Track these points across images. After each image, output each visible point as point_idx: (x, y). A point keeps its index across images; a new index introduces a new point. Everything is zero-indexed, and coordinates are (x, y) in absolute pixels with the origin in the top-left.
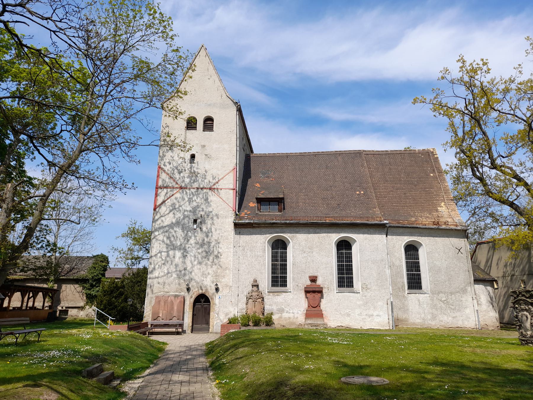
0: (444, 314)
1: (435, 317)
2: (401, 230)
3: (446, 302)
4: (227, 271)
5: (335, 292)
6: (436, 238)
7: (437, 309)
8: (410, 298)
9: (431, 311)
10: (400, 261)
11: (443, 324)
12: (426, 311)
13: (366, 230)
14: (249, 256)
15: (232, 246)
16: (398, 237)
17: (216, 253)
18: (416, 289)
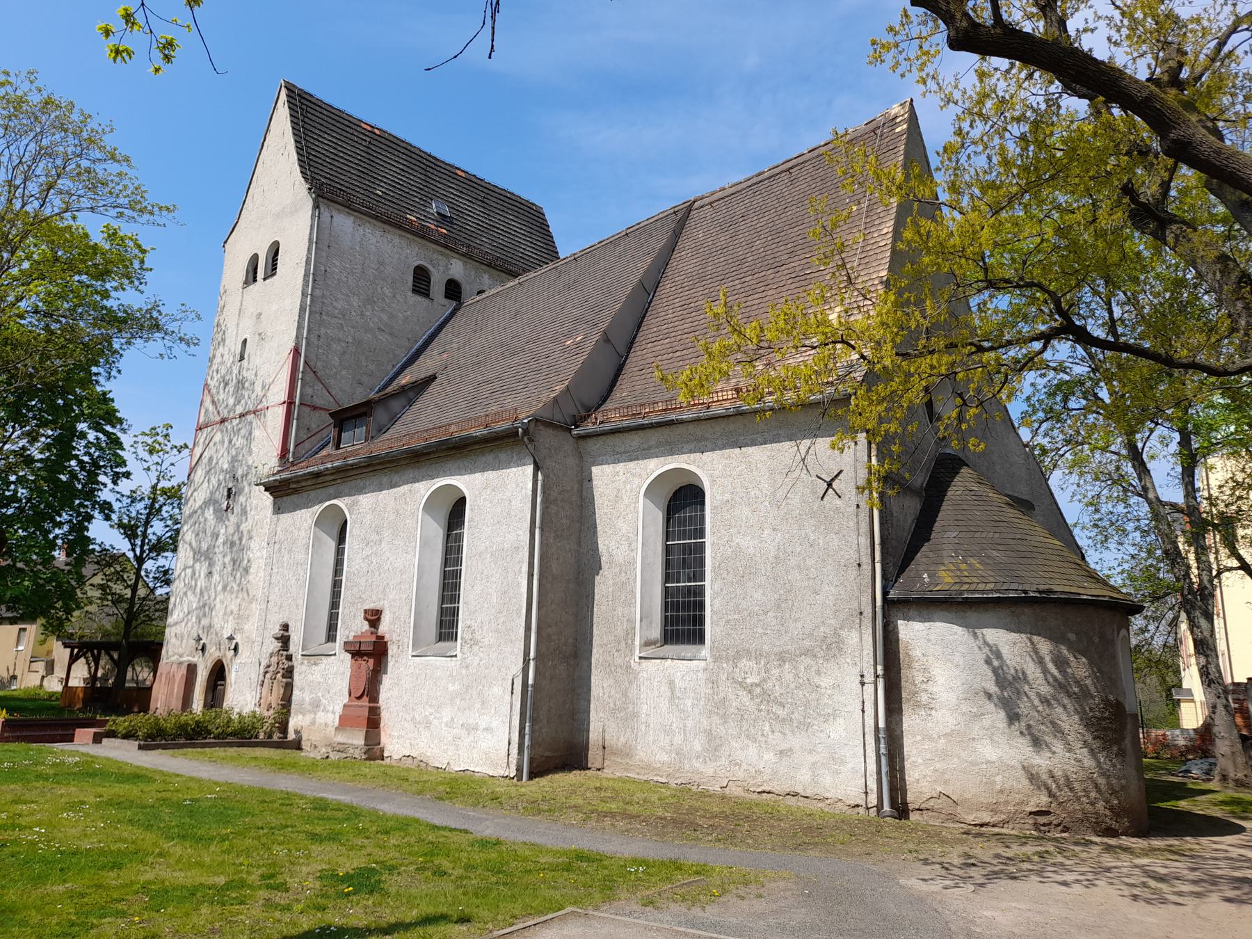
0: (748, 737)
2: (635, 440)
3: (758, 690)
4: (254, 605)
5: (637, 653)
7: (725, 718)
9: (705, 722)
11: (740, 775)
13: (490, 458)
16: (631, 465)
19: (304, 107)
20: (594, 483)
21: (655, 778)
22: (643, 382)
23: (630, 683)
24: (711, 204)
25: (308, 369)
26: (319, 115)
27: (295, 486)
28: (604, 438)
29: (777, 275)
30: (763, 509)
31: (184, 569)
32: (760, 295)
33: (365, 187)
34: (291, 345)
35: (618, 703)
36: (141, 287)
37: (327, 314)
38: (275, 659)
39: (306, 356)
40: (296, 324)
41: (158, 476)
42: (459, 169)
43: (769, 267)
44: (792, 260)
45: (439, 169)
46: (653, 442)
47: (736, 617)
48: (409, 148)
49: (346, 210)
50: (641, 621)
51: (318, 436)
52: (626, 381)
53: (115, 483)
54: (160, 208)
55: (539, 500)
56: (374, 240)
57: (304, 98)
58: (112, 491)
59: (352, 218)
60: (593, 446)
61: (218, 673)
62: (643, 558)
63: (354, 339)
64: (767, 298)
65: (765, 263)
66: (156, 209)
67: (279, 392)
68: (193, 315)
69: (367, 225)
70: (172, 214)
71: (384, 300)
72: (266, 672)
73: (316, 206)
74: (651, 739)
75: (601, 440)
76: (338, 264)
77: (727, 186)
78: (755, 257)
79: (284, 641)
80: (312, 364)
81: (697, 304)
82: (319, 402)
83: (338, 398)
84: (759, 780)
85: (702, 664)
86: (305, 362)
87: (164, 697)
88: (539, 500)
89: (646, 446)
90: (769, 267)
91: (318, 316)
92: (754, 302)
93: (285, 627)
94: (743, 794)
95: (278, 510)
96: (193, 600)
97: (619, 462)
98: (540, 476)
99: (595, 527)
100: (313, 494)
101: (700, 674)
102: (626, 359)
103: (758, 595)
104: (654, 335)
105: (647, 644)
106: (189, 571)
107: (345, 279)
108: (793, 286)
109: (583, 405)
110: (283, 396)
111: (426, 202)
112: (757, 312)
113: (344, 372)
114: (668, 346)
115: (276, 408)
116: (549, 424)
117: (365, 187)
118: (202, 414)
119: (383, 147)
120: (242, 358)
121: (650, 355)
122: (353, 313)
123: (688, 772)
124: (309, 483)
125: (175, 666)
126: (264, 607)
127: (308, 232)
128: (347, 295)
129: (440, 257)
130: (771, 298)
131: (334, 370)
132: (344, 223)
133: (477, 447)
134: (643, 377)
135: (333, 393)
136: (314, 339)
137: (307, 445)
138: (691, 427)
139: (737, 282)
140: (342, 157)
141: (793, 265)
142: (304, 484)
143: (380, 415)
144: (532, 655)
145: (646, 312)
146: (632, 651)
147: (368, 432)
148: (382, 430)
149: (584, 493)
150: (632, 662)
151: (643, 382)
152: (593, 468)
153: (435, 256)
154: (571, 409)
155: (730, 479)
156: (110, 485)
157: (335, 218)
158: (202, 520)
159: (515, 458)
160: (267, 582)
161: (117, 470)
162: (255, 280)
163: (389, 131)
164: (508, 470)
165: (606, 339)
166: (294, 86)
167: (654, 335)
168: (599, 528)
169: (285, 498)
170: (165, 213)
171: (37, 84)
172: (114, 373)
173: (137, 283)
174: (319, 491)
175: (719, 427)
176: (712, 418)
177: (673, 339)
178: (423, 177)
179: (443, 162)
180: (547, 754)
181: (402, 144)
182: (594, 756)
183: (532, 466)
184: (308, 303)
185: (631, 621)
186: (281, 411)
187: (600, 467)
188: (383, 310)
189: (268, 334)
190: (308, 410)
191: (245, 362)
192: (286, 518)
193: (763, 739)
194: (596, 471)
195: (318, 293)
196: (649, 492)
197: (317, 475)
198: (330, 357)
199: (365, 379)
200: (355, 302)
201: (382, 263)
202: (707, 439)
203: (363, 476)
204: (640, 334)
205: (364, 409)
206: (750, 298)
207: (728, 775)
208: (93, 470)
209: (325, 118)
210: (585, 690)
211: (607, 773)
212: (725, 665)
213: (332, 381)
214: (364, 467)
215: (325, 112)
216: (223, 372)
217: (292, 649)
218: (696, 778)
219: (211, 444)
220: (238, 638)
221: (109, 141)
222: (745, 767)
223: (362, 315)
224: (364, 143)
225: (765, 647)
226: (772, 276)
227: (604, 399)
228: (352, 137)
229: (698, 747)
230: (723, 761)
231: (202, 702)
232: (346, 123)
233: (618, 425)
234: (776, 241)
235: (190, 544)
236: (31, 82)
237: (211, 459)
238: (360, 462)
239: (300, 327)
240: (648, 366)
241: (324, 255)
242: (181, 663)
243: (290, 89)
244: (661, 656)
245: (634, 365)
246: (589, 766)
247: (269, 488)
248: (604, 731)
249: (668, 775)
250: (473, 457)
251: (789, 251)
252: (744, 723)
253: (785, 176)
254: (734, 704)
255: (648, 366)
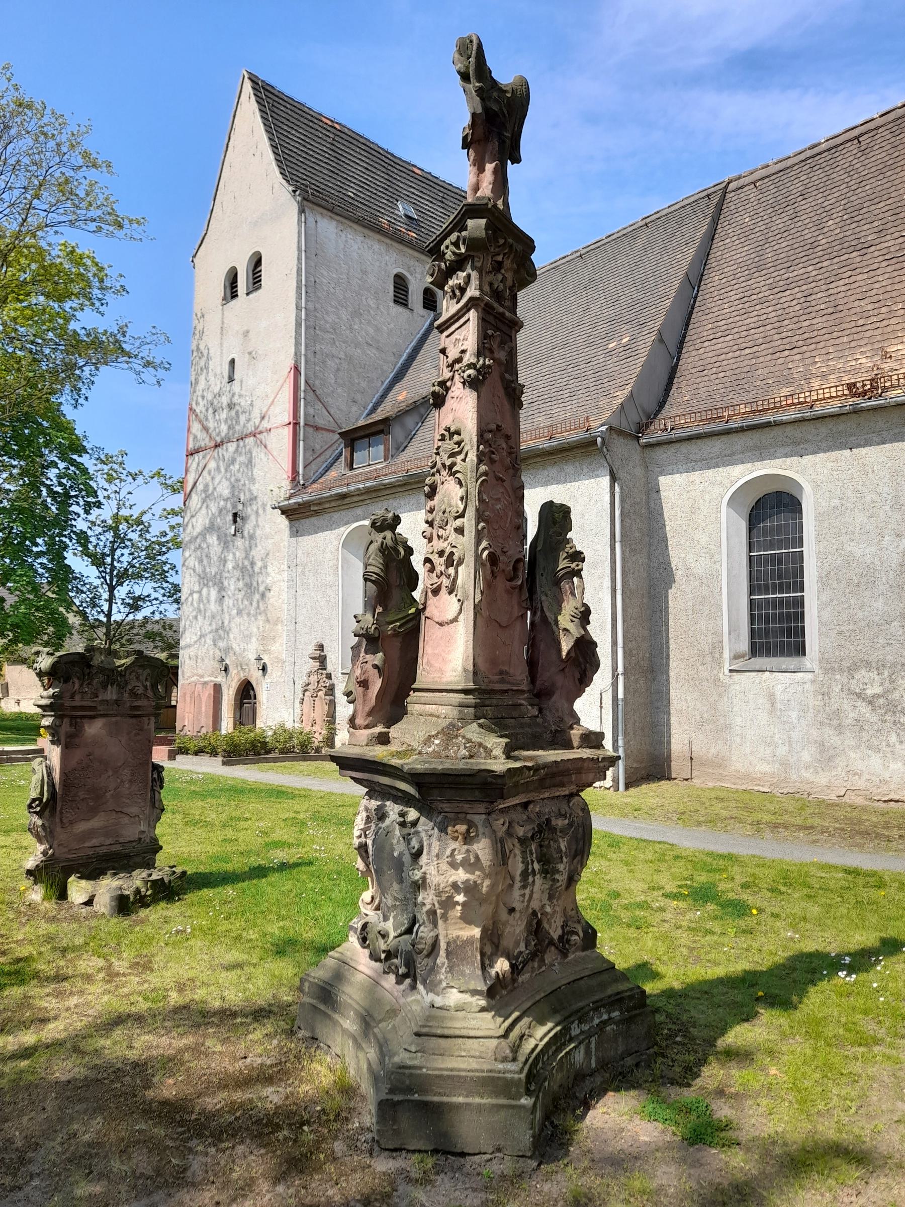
0: (869, 748)
1: (831, 759)
2: (716, 446)
3: (882, 701)
4: (279, 627)
5: (727, 667)
6: (864, 451)
7: (840, 730)
8: (737, 687)
9: (815, 733)
10: (712, 557)
11: (861, 784)
12: (796, 735)
13: (553, 471)
14: (311, 586)
15: (285, 567)
16: (710, 472)
17: (262, 589)
18: (790, 655)
19: (271, 101)
20: (663, 494)
21: (756, 788)
22: (708, 384)
23: (720, 696)
24: (754, 183)
25: (308, 388)
26: (283, 108)
27: (316, 508)
28: (677, 445)
29: (866, 257)
30: (882, 514)
31: (191, 594)
32: (847, 281)
33: (339, 189)
34: (290, 362)
35: (705, 715)
36: (102, 309)
37: (320, 329)
38: (314, 678)
39: (306, 375)
40: (293, 340)
41: (119, 504)
42: (415, 166)
43: (852, 249)
44: (883, 240)
45: (398, 167)
46: (738, 447)
47: (851, 627)
48: (368, 143)
49: (329, 214)
50: (730, 634)
51: (322, 458)
52: (684, 384)
53: (87, 512)
54: (131, 221)
55: (618, 513)
56: (356, 247)
57: (267, 90)
58: (85, 520)
59: (334, 223)
60: (661, 454)
61: (246, 692)
62: (728, 570)
63: (346, 356)
64: (857, 284)
65: (846, 245)
66: (126, 222)
67: (282, 412)
68: (162, 338)
69: (349, 230)
70: (142, 227)
71: (369, 311)
72: (306, 691)
73: (302, 211)
74: (748, 750)
75: (672, 449)
76: (325, 273)
77: (770, 162)
78: (830, 239)
79: (322, 660)
80: (311, 382)
81: (760, 296)
82: (320, 422)
83: (336, 417)
84: (885, 789)
85: (809, 676)
86: (306, 381)
87: (191, 716)
88: (618, 513)
89: (729, 452)
90: (852, 249)
91: (312, 331)
92: (839, 289)
93: (321, 647)
94: (867, 803)
95: (296, 533)
96: (203, 625)
97: (694, 470)
98: (617, 489)
99: (666, 541)
100: (336, 516)
101: (808, 686)
102: (678, 360)
103: (879, 604)
104: (710, 332)
105: (737, 657)
106: (196, 596)
107: (332, 290)
108: (889, 269)
109: (644, 411)
110: (287, 417)
111: (393, 200)
112: (846, 300)
113: (339, 390)
114: (731, 343)
115: (280, 430)
116: (620, 433)
117: (339, 189)
118: (191, 439)
119: (346, 143)
120: (231, 380)
121: (710, 355)
122: (343, 327)
123: (795, 782)
124: (333, 504)
125: (199, 687)
126: (292, 627)
127: (296, 240)
128: (336, 308)
129: (417, 264)
130: (862, 283)
131: (331, 388)
132: (328, 227)
133: (539, 459)
134: (706, 378)
135: (332, 413)
136: (310, 356)
137: (313, 466)
138: (789, 430)
139: (811, 268)
140: (312, 156)
141: (886, 245)
142: (327, 506)
143: (397, 431)
144: (620, 669)
145: (693, 308)
146: (720, 665)
147: (387, 451)
148: (401, 448)
149: (652, 505)
150: (721, 675)
151: (708, 384)
152: (661, 479)
153: (412, 263)
154: (634, 416)
155: (838, 483)
156: (83, 516)
157: (319, 223)
158: (204, 546)
159: (586, 470)
160: (293, 605)
161: (89, 500)
162: (234, 295)
163: (348, 126)
164: (578, 484)
165: (661, 340)
166: (257, 77)
167: (710, 332)
168: (671, 542)
169: (303, 521)
170: (135, 226)
171: (13, 82)
172: (81, 401)
173: (97, 304)
174: (343, 513)
175: (823, 429)
176: (814, 419)
177: (737, 336)
178: (386, 177)
179: (400, 159)
180: (635, 765)
181: (361, 140)
182: (678, 767)
183: (608, 478)
184: (303, 317)
185: (718, 634)
186: (287, 432)
187: (670, 477)
188: (369, 322)
189: (260, 352)
190: (310, 430)
191: (236, 386)
192: (308, 542)
193: (888, 749)
194: (664, 481)
195: (311, 306)
196: (732, 501)
197: (343, 496)
198: (326, 374)
199: (358, 397)
200: (344, 315)
201: (364, 272)
202: (807, 441)
203: (397, 495)
204: (690, 333)
205: (381, 427)
206: (832, 286)
207: (845, 784)
208: (64, 499)
209: (290, 112)
210: (665, 703)
211: (696, 782)
212: (838, 677)
213: (329, 399)
214: (399, 486)
215: (288, 106)
216: (209, 397)
217: (330, 668)
218: (807, 788)
219: (205, 473)
220: (266, 659)
221: (89, 143)
222: (866, 776)
223: (351, 328)
224: (328, 140)
225: (890, 658)
226: (859, 259)
227: (661, 405)
228: (316, 133)
229: (806, 756)
230: (840, 771)
231: (231, 721)
232: (309, 117)
233: (696, 430)
234: (856, 219)
235: (194, 570)
236: (9, 80)
237: (206, 486)
238: (397, 481)
239: (297, 344)
240: (709, 366)
241: (313, 265)
242: (205, 683)
243: (254, 80)
244: (758, 668)
245: (690, 366)
246: (673, 776)
247: (285, 511)
248: (691, 743)
249: (771, 785)
250: (532, 471)
251: (876, 230)
252: (864, 734)
253: (853, 147)
254: (851, 715)
255: (709, 366)
